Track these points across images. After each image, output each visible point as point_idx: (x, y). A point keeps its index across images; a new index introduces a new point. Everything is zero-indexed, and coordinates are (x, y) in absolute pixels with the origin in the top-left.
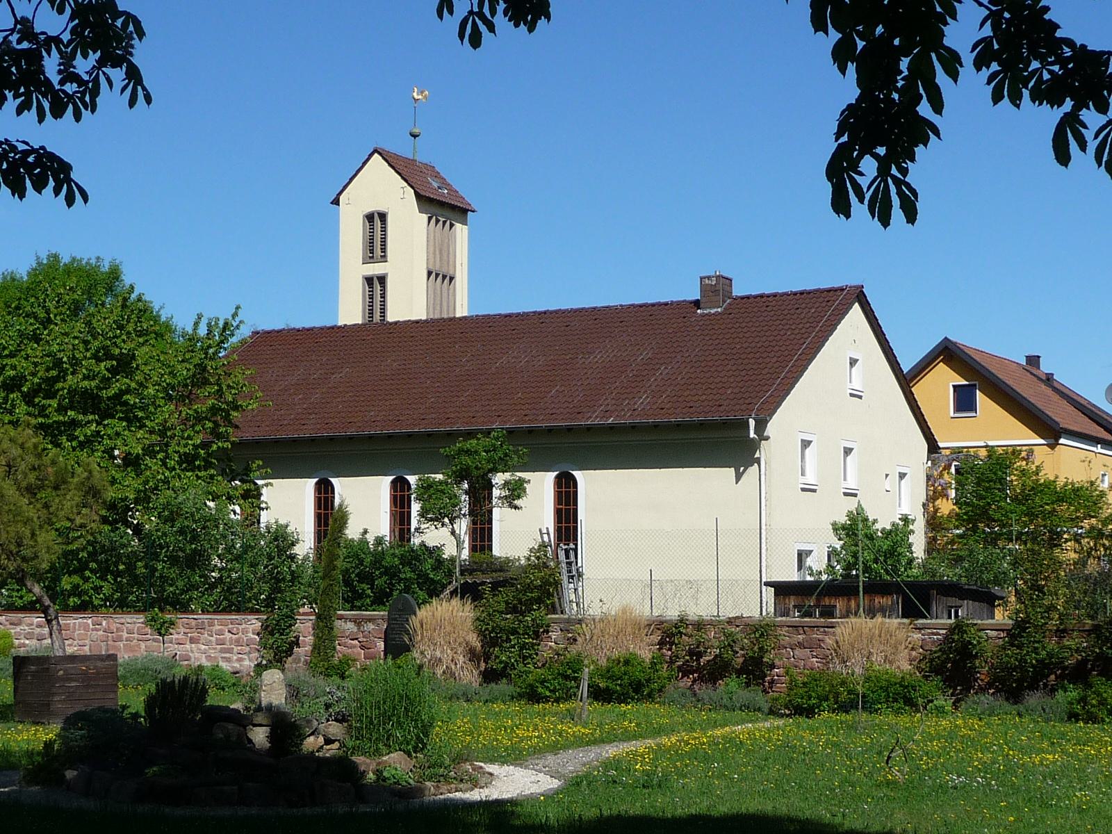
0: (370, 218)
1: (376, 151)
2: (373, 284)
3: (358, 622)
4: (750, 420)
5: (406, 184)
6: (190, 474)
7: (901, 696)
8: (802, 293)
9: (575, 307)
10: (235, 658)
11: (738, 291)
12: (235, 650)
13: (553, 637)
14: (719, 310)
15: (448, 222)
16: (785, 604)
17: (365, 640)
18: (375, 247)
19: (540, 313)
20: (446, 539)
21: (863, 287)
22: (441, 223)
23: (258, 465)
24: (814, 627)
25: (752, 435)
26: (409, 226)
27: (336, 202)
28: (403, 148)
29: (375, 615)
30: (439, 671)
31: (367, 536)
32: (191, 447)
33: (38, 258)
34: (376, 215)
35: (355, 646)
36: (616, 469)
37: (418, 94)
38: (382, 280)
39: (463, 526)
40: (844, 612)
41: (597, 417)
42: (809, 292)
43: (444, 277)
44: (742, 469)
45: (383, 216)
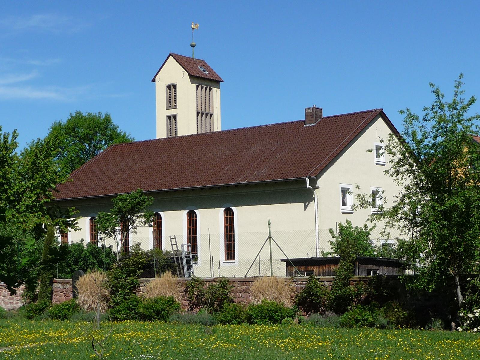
0: (169, 87)
1: (170, 55)
2: (171, 119)
3: (63, 284)
4: (307, 179)
5: (184, 70)
6: (32, 215)
7: (272, 315)
8: (354, 114)
9: (251, 126)
10: (15, 302)
11: (325, 114)
12: (15, 299)
13: (141, 289)
14: (314, 124)
15: (209, 87)
16: (291, 270)
17: (66, 292)
18: (171, 103)
19: (235, 130)
20: (112, 242)
21: (382, 109)
22: (204, 88)
23: (73, 209)
24: (250, 282)
25: (308, 186)
26: (187, 90)
27: (154, 80)
28: (187, 53)
29: (70, 280)
30: (86, 307)
31: (83, 242)
32: (31, 202)
33: (71, 114)
34: (171, 86)
35: (61, 296)
36: (241, 206)
37: (194, 26)
38: (175, 117)
39: (119, 236)
40: (317, 273)
41: (240, 180)
42: (357, 114)
43: (207, 115)
44: (307, 203)
45: (175, 86)
